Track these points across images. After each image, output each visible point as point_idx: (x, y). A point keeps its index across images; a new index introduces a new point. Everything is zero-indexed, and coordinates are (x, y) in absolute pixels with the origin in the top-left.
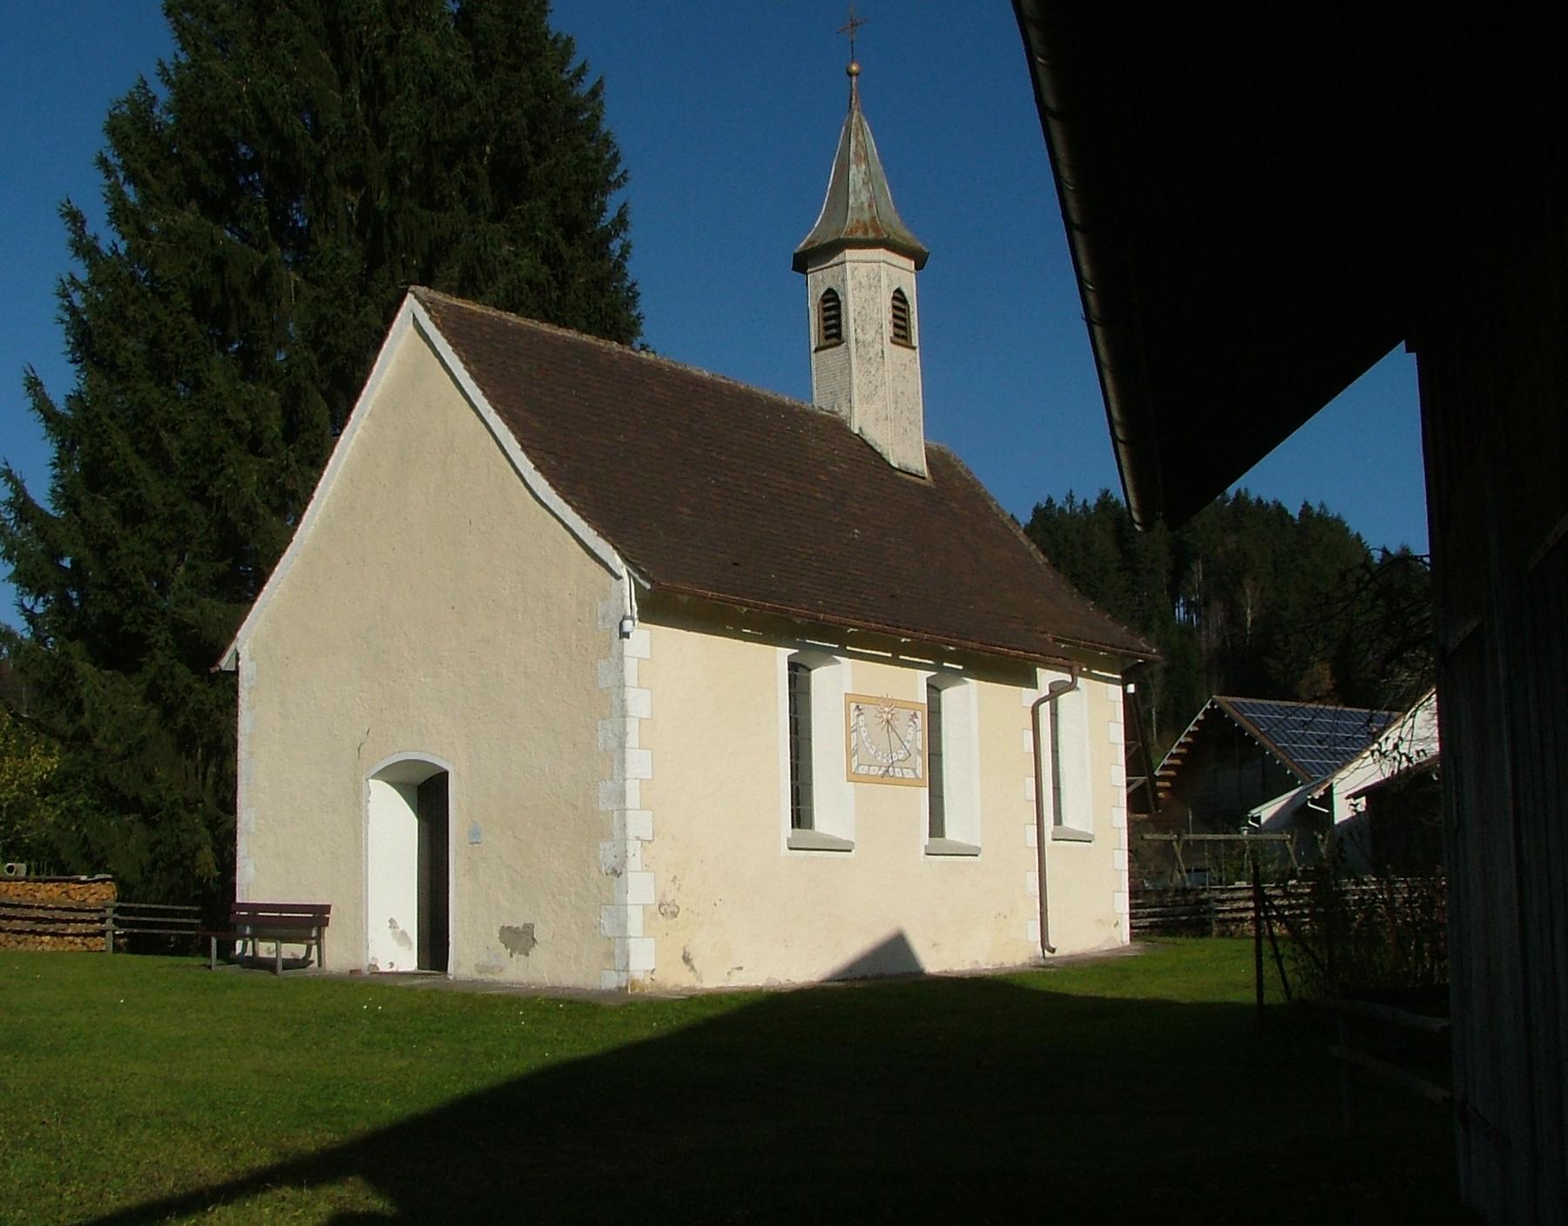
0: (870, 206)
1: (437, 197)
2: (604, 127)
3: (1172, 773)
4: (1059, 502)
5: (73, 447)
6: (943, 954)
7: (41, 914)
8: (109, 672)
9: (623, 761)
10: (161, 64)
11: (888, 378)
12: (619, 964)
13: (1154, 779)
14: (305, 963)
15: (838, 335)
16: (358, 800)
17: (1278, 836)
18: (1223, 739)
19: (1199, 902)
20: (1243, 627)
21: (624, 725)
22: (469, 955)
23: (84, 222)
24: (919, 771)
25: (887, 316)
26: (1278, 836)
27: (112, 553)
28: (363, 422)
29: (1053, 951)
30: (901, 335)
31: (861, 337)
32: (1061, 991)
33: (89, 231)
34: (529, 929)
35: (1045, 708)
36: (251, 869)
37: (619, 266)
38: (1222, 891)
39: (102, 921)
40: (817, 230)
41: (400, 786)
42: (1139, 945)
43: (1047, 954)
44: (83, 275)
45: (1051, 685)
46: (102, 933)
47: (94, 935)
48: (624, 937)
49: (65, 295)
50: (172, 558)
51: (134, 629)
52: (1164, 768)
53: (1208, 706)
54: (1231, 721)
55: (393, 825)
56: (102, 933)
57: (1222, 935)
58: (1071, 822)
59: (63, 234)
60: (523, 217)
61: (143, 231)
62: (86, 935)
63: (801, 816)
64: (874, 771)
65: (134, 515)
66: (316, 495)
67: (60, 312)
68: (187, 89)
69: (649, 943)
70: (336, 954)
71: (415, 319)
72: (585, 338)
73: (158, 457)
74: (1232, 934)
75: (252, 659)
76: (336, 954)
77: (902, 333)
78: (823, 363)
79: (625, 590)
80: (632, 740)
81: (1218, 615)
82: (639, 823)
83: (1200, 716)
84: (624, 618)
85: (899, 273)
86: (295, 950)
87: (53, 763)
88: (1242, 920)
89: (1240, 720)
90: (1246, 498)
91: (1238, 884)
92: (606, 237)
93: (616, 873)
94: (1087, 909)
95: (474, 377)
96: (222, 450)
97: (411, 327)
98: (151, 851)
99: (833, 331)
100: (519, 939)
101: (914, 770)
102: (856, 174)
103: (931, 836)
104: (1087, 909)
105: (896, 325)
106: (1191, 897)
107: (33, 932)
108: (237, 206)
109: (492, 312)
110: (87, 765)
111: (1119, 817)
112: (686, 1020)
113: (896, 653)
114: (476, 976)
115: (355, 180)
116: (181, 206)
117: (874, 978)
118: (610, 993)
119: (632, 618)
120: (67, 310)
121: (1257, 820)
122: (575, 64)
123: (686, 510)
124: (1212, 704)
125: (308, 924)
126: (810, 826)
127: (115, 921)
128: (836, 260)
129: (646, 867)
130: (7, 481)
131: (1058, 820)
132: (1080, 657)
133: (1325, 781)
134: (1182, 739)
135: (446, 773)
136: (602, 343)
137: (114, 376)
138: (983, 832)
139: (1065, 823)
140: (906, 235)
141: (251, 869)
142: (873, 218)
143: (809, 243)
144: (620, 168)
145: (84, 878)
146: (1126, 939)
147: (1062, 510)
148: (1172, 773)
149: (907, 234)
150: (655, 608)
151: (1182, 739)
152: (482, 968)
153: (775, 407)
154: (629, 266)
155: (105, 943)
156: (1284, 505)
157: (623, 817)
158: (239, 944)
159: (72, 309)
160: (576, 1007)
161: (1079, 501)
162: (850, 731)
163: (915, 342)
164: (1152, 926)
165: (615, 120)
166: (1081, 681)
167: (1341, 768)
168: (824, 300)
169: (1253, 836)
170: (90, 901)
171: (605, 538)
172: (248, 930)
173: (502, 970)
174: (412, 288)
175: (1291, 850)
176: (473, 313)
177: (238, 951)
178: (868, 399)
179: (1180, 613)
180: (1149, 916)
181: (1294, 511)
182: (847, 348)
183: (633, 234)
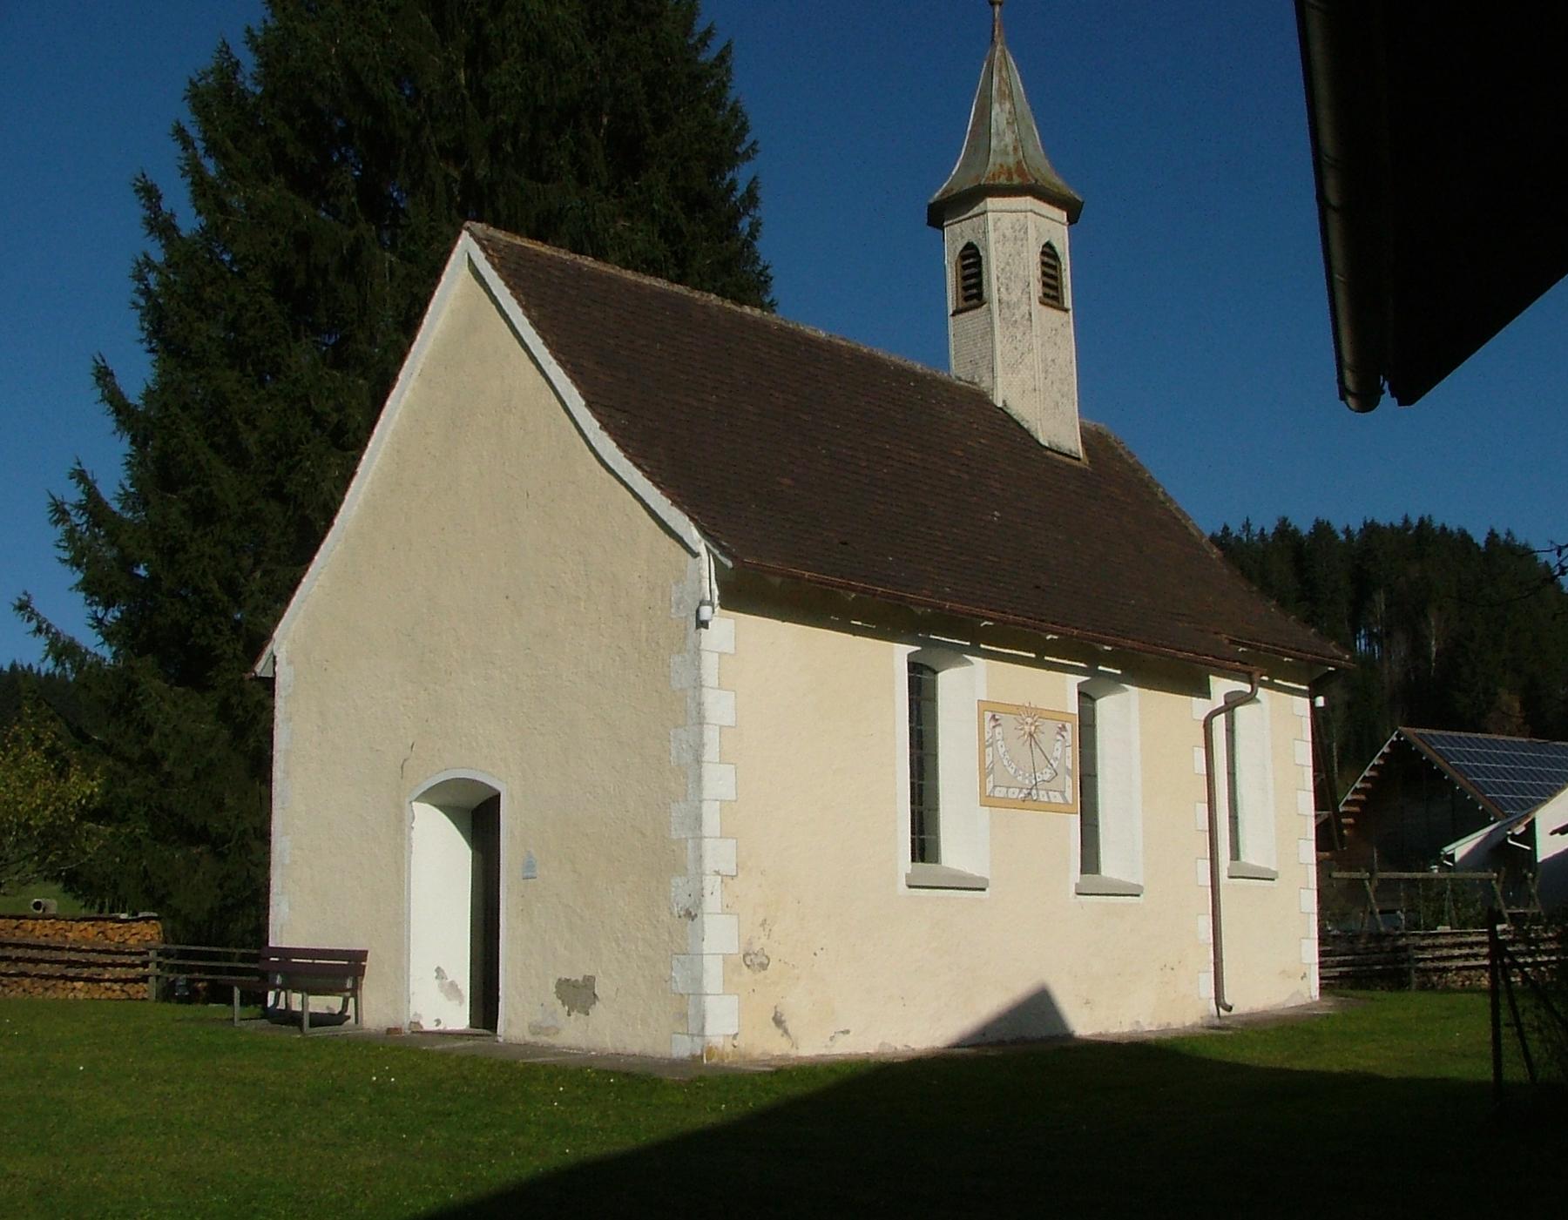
0: (1015, 149)
1: (545, 169)
2: (732, 95)
3: (1356, 809)
4: (1235, 529)
5: (145, 444)
6: (1090, 1017)
7: (74, 956)
8: (181, 689)
9: (700, 777)
10: (249, 30)
11: (1037, 343)
12: (693, 1027)
13: (1338, 815)
14: (337, 1019)
15: (979, 296)
16: (400, 826)
17: (1483, 875)
18: (1410, 772)
19: (1397, 949)
20: (1427, 659)
21: (701, 734)
22: (518, 1019)
23: (160, 197)
24: (1069, 795)
25: (1035, 272)
26: (1483, 875)
27: (180, 557)
28: (412, 383)
29: (1230, 1009)
30: (1052, 296)
31: (1005, 297)
32: (1240, 1060)
33: (166, 206)
34: (589, 981)
35: (1220, 722)
36: (285, 908)
37: (748, 244)
38: (1423, 937)
39: (145, 965)
40: (956, 176)
41: (453, 812)
42: (1330, 1001)
43: (1222, 1011)
44: (158, 256)
45: (1226, 696)
46: (145, 979)
47: (135, 981)
48: (700, 994)
49: (140, 277)
50: (247, 562)
51: (203, 642)
52: (1348, 803)
53: (1394, 738)
54: (1419, 753)
55: (439, 854)
56: (145, 979)
57: (1422, 987)
58: (1249, 856)
59: (136, 210)
60: (640, 192)
61: (222, 207)
62: (126, 981)
63: (924, 846)
64: (1014, 793)
65: (205, 514)
66: (359, 470)
67: (136, 297)
68: (272, 51)
69: (732, 1002)
70: (375, 1009)
71: (470, 259)
72: (677, 288)
73: (238, 458)
74: (1433, 986)
75: (290, 663)
76: (375, 1009)
77: (1052, 293)
78: (961, 329)
79: (704, 570)
80: (711, 753)
81: (1401, 649)
82: (718, 854)
83: (1385, 749)
84: (702, 603)
85: (1051, 225)
86: (332, 1003)
87: (94, 787)
88: (1446, 970)
89: (1428, 753)
90: (1429, 525)
91: (1440, 929)
92: (736, 216)
93: (690, 915)
94: (1277, 962)
95: (535, 324)
96: (299, 441)
97: (466, 270)
98: (220, 886)
99: (973, 292)
100: (577, 994)
101: (1062, 793)
102: (999, 114)
103: (1083, 872)
104: (1277, 962)
105: (1045, 284)
106: (1386, 944)
107: (65, 978)
108: (327, 181)
109: (565, 255)
110: (152, 791)
111: (1308, 851)
112: (766, 1100)
113: (1041, 653)
114: (530, 1039)
115: (457, 153)
116: (266, 180)
117: (1013, 1042)
118: (675, 1064)
119: (711, 603)
120: (142, 294)
121: (1451, 857)
122: (699, 27)
123: (787, 481)
124: (1398, 736)
125: (342, 973)
126: (936, 859)
127: (159, 965)
128: (976, 210)
129: (727, 909)
130: (79, 483)
131: (1235, 854)
132: (1261, 663)
133: (1527, 816)
134: (1366, 773)
135: (499, 796)
136: (697, 295)
137: (188, 364)
138: (1162, 867)
139: (1243, 858)
140: (1057, 182)
141: (285, 908)
142: (1019, 163)
143: (946, 191)
144: (749, 138)
145: (124, 916)
146: (1315, 993)
147: (1238, 539)
148: (1356, 809)
149: (1058, 181)
150: (741, 593)
151: (1366, 773)
152: (536, 1029)
153: (903, 374)
154: (760, 246)
155: (149, 990)
156: (1470, 532)
157: (699, 847)
158: (271, 995)
159: (147, 293)
160: (631, 1081)
161: (1256, 529)
162: (983, 745)
163: (1068, 303)
164: (1342, 976)
165: (745, 88)
166: (1262, 693)
167: (1543, 802)
168: (963, 257)
169: (1445, 875)
170: (132, 942)
171: (680, 508)
172: (279, 980)
173: (558, 1031)
174: (468, 224)
175: (1498, 888)
176: (538, 254)
177: (270, 1003)
178: (1013, 368)
179: (1361, 644)
180: (1340, 964)
181: (1480, 539)
182: (989, 310)
183: (762, 212)
